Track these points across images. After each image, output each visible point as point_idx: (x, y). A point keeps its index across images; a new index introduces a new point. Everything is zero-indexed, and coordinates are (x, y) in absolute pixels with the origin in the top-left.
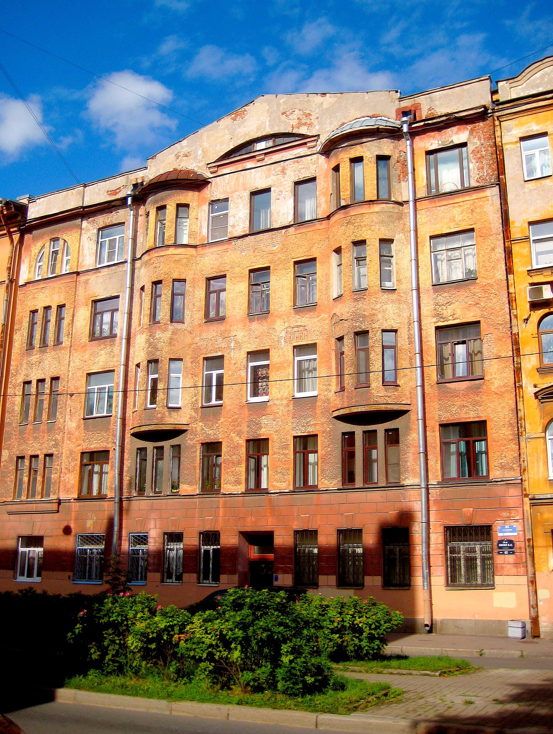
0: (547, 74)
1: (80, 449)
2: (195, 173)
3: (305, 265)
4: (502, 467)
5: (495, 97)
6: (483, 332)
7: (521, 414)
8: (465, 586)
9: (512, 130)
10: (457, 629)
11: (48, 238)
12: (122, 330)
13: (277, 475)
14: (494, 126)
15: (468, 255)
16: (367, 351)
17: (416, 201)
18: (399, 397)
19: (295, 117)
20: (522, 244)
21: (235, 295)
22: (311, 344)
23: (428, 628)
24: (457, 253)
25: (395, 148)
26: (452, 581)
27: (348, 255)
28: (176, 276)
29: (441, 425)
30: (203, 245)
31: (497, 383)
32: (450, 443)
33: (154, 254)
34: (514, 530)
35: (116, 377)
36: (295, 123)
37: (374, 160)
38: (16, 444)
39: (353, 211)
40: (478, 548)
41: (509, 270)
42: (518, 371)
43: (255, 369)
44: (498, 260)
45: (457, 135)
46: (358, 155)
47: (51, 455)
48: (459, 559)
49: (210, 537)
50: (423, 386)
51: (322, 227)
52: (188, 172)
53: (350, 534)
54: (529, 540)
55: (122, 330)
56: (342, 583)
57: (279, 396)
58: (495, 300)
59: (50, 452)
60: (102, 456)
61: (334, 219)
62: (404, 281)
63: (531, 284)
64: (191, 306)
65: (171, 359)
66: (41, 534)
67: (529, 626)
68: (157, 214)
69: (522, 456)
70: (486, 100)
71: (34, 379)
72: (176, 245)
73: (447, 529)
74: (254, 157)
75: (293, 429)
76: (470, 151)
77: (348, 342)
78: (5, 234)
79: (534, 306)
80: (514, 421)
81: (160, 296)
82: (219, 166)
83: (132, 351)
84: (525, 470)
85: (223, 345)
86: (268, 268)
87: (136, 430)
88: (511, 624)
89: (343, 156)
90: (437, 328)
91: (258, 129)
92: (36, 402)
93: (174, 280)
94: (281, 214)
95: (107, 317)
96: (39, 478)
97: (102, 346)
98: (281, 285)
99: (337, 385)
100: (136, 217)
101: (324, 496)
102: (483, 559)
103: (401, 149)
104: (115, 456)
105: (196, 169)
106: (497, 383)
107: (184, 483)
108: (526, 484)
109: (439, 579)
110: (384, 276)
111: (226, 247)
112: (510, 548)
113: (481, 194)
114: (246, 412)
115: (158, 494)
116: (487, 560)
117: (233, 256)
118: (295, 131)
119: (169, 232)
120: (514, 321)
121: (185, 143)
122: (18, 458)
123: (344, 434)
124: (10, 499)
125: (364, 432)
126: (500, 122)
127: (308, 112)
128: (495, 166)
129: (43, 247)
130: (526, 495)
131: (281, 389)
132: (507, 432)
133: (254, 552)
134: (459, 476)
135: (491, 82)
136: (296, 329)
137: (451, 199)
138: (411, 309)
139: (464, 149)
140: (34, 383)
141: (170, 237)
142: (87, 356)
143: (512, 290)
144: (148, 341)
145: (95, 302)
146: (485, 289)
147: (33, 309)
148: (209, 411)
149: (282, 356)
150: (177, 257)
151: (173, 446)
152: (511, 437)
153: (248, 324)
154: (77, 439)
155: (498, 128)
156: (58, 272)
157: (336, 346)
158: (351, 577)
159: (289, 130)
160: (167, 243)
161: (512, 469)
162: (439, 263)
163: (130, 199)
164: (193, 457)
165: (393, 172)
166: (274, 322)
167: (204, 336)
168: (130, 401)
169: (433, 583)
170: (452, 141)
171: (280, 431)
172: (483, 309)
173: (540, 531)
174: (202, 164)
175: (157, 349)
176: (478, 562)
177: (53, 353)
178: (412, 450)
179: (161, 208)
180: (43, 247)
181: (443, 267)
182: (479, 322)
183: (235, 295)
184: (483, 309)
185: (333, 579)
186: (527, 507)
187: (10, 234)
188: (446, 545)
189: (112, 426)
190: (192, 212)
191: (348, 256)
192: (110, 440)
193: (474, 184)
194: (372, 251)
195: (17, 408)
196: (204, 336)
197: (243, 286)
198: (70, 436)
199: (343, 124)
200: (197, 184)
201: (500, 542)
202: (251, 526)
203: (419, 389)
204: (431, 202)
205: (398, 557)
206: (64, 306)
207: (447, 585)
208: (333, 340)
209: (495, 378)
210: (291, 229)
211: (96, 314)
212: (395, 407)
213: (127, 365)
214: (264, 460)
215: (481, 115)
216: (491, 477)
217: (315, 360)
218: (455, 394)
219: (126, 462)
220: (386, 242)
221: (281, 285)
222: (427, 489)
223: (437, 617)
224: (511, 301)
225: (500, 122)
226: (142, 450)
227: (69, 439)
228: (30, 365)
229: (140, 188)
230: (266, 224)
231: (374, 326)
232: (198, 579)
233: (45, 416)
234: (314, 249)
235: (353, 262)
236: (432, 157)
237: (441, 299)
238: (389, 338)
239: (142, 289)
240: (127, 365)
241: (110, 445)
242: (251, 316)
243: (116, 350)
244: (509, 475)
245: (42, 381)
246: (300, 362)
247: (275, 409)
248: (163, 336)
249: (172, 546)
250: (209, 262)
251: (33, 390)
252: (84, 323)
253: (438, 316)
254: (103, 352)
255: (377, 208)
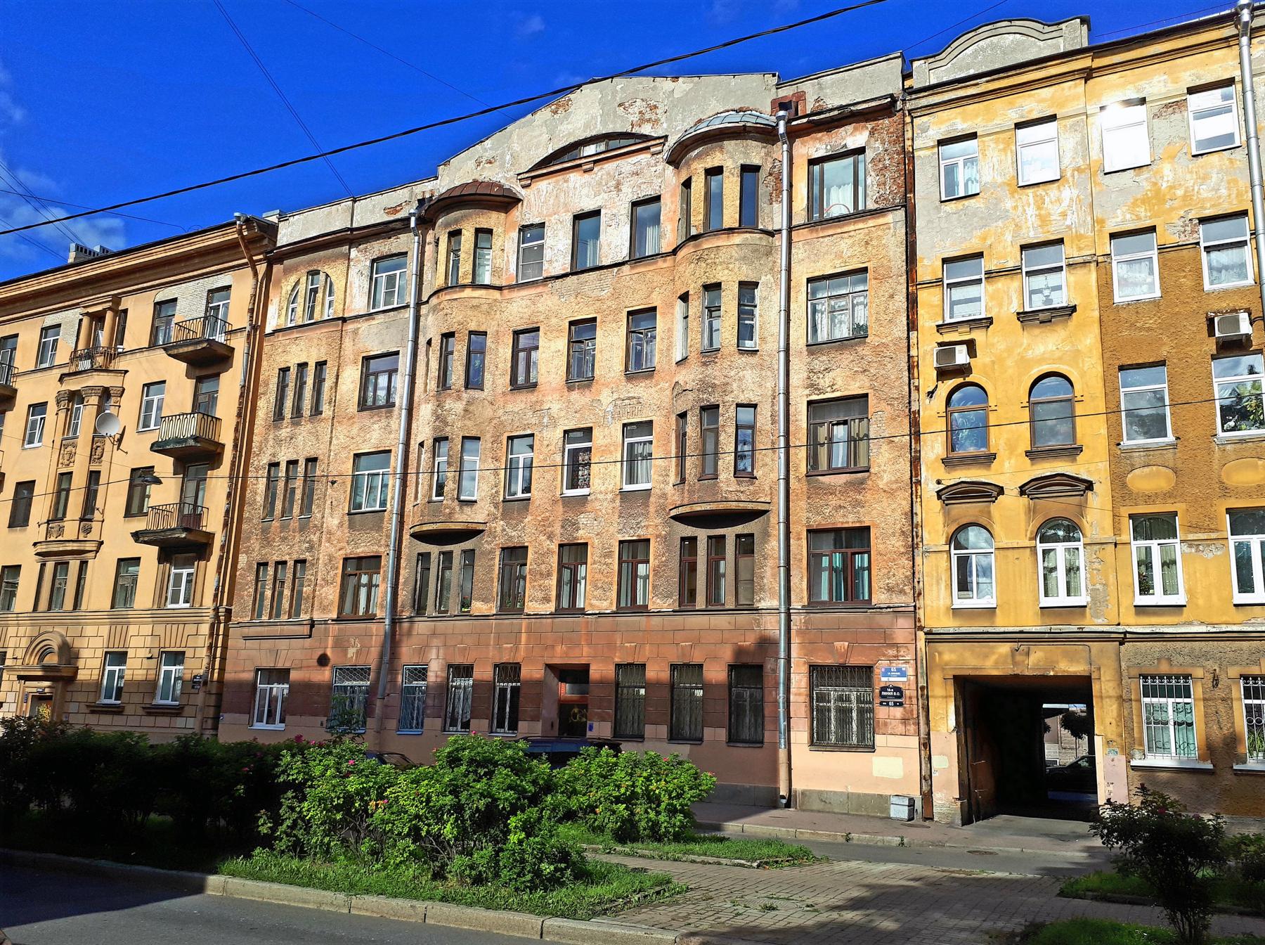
0: (983, 49)
1: (342, 554)
2: (501, 186)
3: (642, 318)
4: (890, 589)
5: (908, 83)
6: (871, 410)
7: (917, 519)
8: (835, 745)
9: (929, 130)
10: (823, 805)
11: (304, 271)
12: (402, 397)
13: (597, 594)
14: (904, 124)
15: (858, 304)
16: (716, 432)
17: (790, 229)
18: (755, 493)
19: (637, 110)
20: (932, 290)
21: (551, 356)
22: (646, 422)
23: (784, 801)
24: (842, 303)
25: (767, 154)
26: (818, 740)
27: (697, 303)
28: (473, 327)
29: (809, 531)
30: (510, 287)
31: (886, 477)
32: (822, 555)
33: (445, 297)
34: (903, 674)
35: (392, 458)
36: (635, 118)
37: (738, 171)
38: (257, 546)
39: (707, 244)
40: (853, 697)
41: (912, 325)
42: (915, 462)
43: (574, 454)
44: (898, 311)
45: (854, 137)
46: (716, 164)
47: (303, 562)
48: (829, 710)
49: (509, 670)
50: (787, 479)
51: (665, 265)
52: (492, 185)
53: (688, 670)
54: (922, 688)
55: (402, 397)
56: (675, 736)
57: (603, 489)
58: (890, 366)
59: (302, 557)
60: (371, 562)
61: (681, 254)
62: (769, 339)
63: (940, 344)
64: (493, 368)
65: (464, 438)
66: (287, 665)
67: (918, 805)
68: (449, 241)
69: (917, 575)
70: (895, 87)
71: (283, 459)
72: (474, 285)
73: (813, 668)
74: (580, 165)
75: (619, 531)
76: (868, 160)
77: (692, 419)
78: (246, 264)
79: (943, 374)
80: (907, 528)
81: (452, 353)
82: (533, 178)
83: (414, 426)
84: (920, 594)
85: (533, 421)
86: (594, 319)
87: (417, 529)
88: (894, 800)
89: (697, 167)
90: (810, 403)
91: (587, 126)
92: (286, 490)
93: (471, 333)
94: (613, 246)
95: (383, 380)
96: (287, 592)
97: (376, 418)
98: (610, 345)
99: (677, 475)
100: (422, 245)
101: (655, 621)
102: (861, 712)
103: (775, 156)
104: (388, 563)
105: (503, 181)
106: (886, 477)
107: (478, 600)
108: (920, 613)
109: (800, 736)
110: (745, 332)
111: (540, 289)
112: (897, 697)
113: (881, 221)
114: (560, 508)
115: (442, 613)
116: (866, 715)
117: (549, 303)
118: (636, 130)
119: (465, 267)
120: (914, 394)
121: (488, 143)
122: (259, 564)
123: (683, 539)
124: (247, 619)
125: (710, 537)
126: (912, 118)
127: (653, 103)
128: (901, 181)
129: (297, 283)
130: (921, 628)
131: (606, 477)
132: (898, 544)
133: (565, 690)
134: (831, 598)
135: (904, 61)
136: (627, 402)
137: (840, 227)
138: (776, 377)
139: (861, 157)
140: (283, 466)
141: (465, 274)
142: (355, 431)
143: (913, 352)
144: (435, 412)
145: (367, 359)
146: (878, 350)
147: (283, 366)
148: (513, 506)
149: (608, 440)
150: (475, 302)
151: (464, 552)
152: (902, 550)
153: (566, 393)
154: (339, 541)
155: (909, 127)
156: (317, 317)
157: (677, 425)
158: (687, 728)
159: (627, 128)
160: (461, 282)
161: (902, 592)
162: (818, 316)
163: (413, 219)
164: (490, 568)
165: (762, 190)
166: (599, 392)
167: (509, 407)
168: (410, 491)
169: (792, 741)
170: (845, 146)
171: (602, 530)
172: (874, 378)
173: (937, 677)
174: (511, 173)
175: (446, 424)
176: (854, 714)
177: (309, 426)
178: (770, 563)
179: (455, 234)
180: (297, 283)
181: (823, 321)
182: (866, 395)
183: (551, 356)
184: (874, 378)
185: (663, 730)
186: (921, 644)
187: (253, 264)
188: (811, 690)
189: (385, 524)
190: (497, 242)
191: (696, 305)
192: (383, 542)
193: (871, 205)
194: (729, 301)
195: (260, 499)
196: (509, 407)
197: (562, 344)
198: (332, 536)
199: (700, 121)
200: (507, 202)
201: (884, 689)
202: (560, 656)
203: (782, 482)
204: (812, 232)
205: (747, 703)
206: (325, 363)
207: (812, 743)
208: (674, 417)
209: (884, 471)
210: (626, 268)
211: (367, 376)
212: (750, 506)
213: (407, 445)
214: (582, 570)
215: (885, 109)
216: (874, 602)
217: (651, 442)
218: (830, 491)
219: (402, 572)
220: (747, 288)
221: (610, 345)
222: (788, 615)
223: (798, 786)
224: (912, 366)
225: (912, 118)
226: (424, 557)
227: (329, 540)
228: (279, 442)
229: (426, 206)
230: (594, 261)
231: (727, 398)
232: (491, 726)
233: (296, 510)
234: (654, 295)
235: (703, 312)
236: (817, 168)
237: (818, 365)
238: (746, 415)
239: (429, 343)
240: (407, 445)
241: (382, 549)
242: (570, 385)
243: (394, 423)
244: (898, 600)
245: (295, 462)
246: (631, 445)
247: (597, 505)
248: (455, 406)
249: (457, 682)
250: (518, 308)
251: (282, 473)
252: (352, 386)
253: (813, 386)
254: (376, 426)
255: (737, 239)
